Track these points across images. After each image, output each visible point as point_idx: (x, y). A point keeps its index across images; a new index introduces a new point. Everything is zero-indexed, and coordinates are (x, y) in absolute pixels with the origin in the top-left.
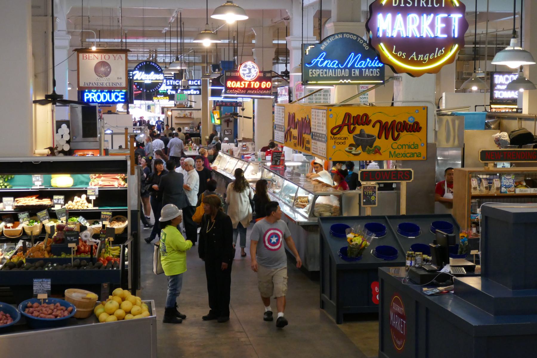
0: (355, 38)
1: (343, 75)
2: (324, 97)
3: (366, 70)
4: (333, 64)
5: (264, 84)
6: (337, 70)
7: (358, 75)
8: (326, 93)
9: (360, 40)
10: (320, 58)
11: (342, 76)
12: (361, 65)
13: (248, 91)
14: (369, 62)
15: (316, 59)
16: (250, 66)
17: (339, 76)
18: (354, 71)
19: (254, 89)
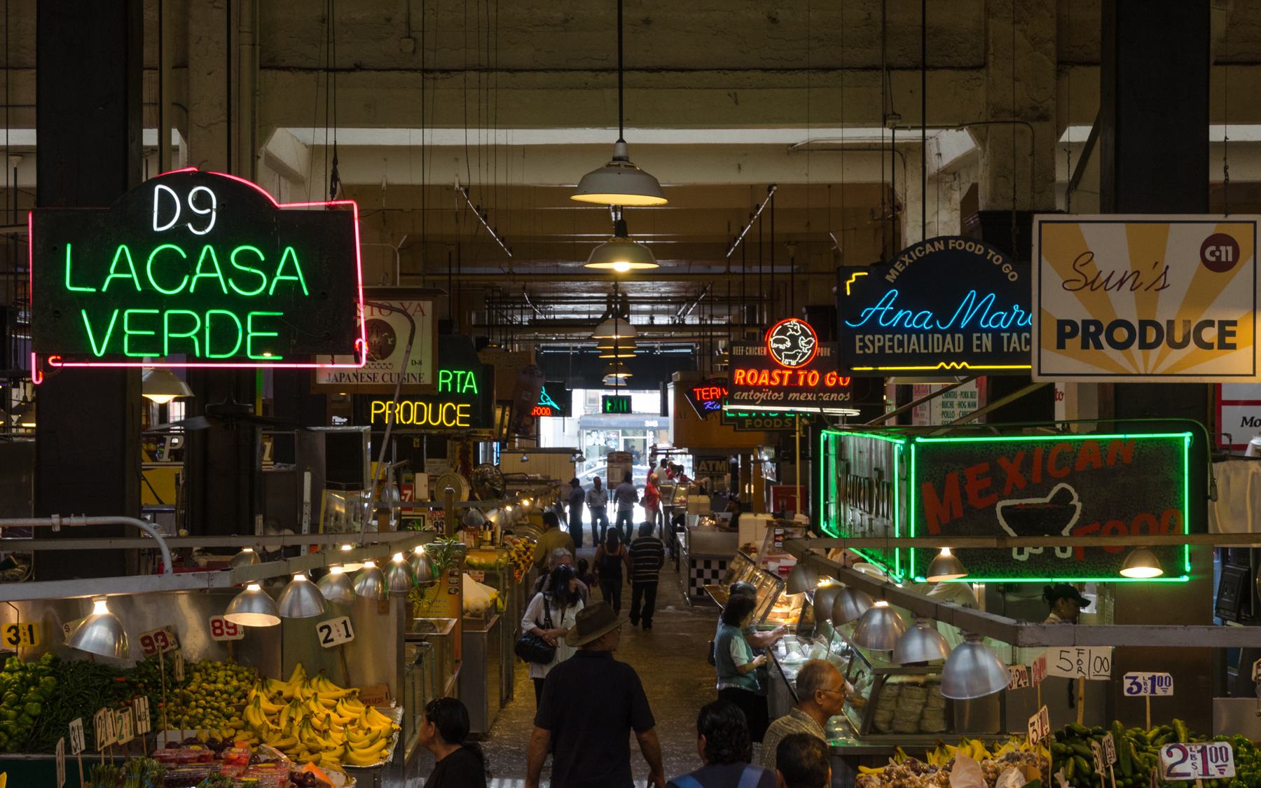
0: (980, 250)
1: (949, 349)
2: (944, 410)
3: (1011, 336)
4: (919, 321)
5: (1008, 267)
6: (930, 336)
7: (990, 350)
8: (951, 400)
9: (993, 256)
10: (884, 305)
11: (945, 351)
12: (996, 321)
13: (791, 395)
14: (1018, 315)
15: (874, 307)
16: (797, 331)
17: (936, 351)
18: (979, 339)
19: (806, 388)
